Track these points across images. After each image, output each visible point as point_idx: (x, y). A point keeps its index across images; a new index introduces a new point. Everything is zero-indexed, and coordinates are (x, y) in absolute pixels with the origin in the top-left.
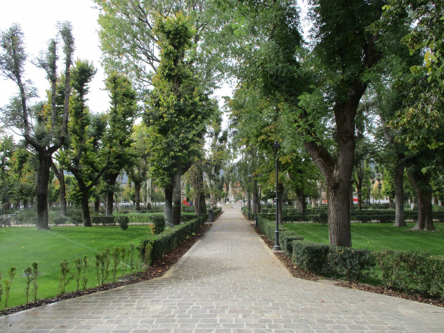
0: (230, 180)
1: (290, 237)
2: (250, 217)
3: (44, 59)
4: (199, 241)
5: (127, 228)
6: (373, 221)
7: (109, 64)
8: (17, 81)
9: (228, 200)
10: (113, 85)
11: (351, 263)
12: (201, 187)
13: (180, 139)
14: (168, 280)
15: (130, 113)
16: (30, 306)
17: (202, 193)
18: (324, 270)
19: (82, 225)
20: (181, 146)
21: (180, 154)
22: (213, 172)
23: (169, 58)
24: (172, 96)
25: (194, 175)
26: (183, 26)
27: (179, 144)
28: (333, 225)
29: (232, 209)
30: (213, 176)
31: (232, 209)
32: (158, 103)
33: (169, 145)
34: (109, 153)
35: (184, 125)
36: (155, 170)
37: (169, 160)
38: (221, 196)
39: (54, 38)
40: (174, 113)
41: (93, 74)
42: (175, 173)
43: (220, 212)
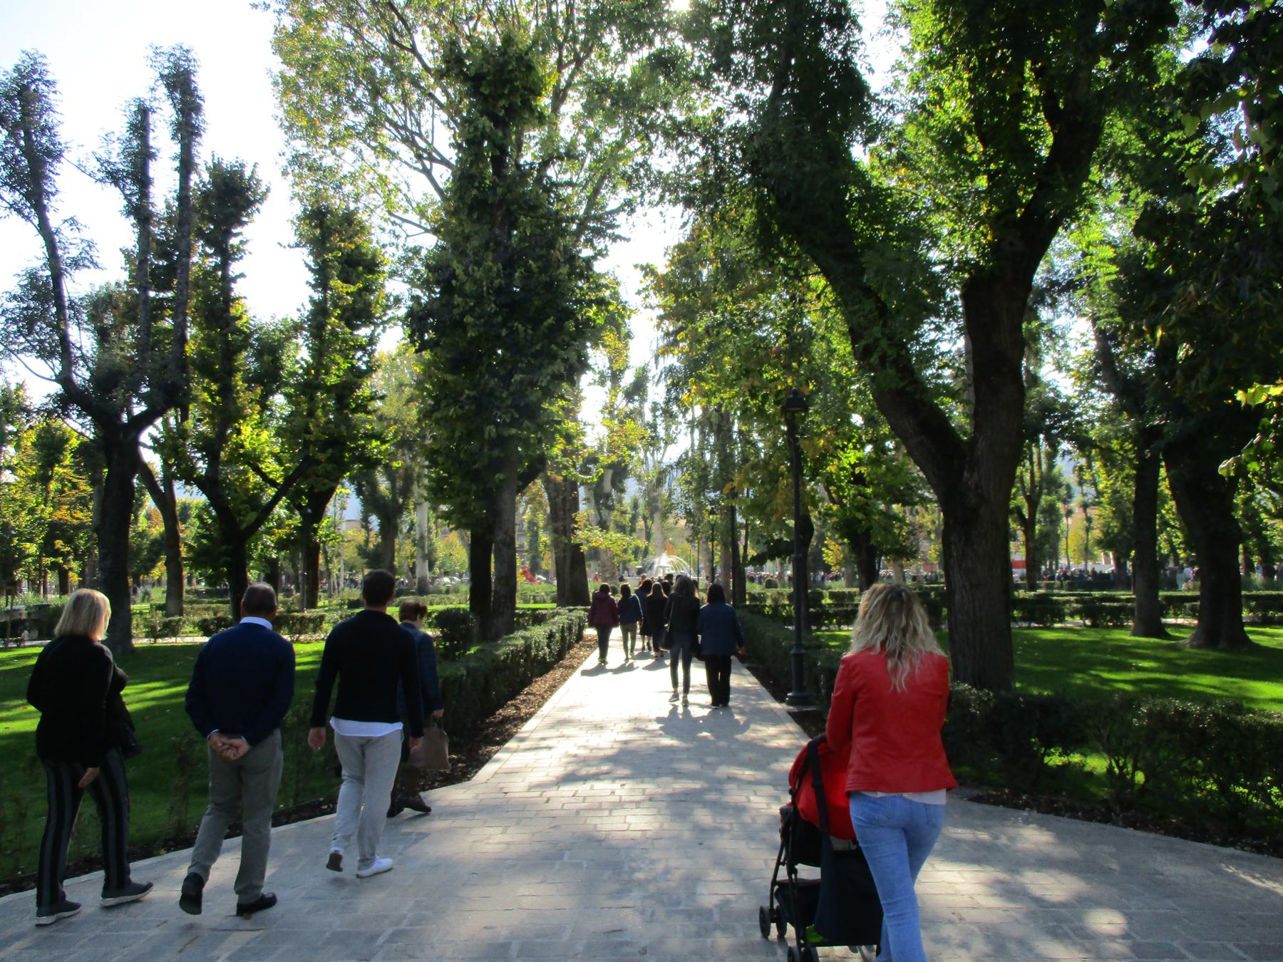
3: (114, 159)
13: (512, 389)
27: (509, 402)
39: (145, 95)
40: (496, 314)
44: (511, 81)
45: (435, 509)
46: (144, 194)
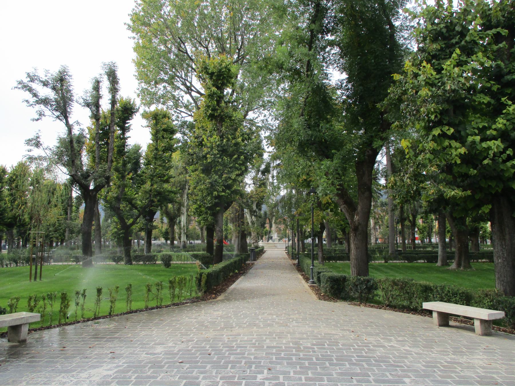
0: (274, 216)
1: (320, 271)
2: (293, 256)
3: (88, 99)
4: (242, 277)
5: (170, 266)
6: (419, 261)
7: (151, 98)
8: (64, 121)
9: (271, 238)
10: (155, 121)
11: (361, 288)
12: (243, 225)
13: (223, 179)
14: (222, 301)
15: (170, 149)
16: (127, 313)
17: (243, 232)
18: (343, 295)
19: (123, 263)
20: (224, 186)
21: (223, 194)
22: (254, 207)
23: (212, 99)
24: (215, 136)
25: (235, 212)
26: (226, 67)
27: (222, 184)
28: (353, 260)
29: (275, 248)
30: (255, 211)
31: (275, 248)
32: (201, 142)
33: (213, 185)
34: (151, 191)
35: (227, 165)
36: (196, 209)
37: (211, 199)
38: (263, 233)
39: (98, 76)
40: (218, 154)
41: (135, 112)
42: (218, 212)
43: (261, 252)
44: (223, 75)
45: (357, 276)
46: (98, 110)
